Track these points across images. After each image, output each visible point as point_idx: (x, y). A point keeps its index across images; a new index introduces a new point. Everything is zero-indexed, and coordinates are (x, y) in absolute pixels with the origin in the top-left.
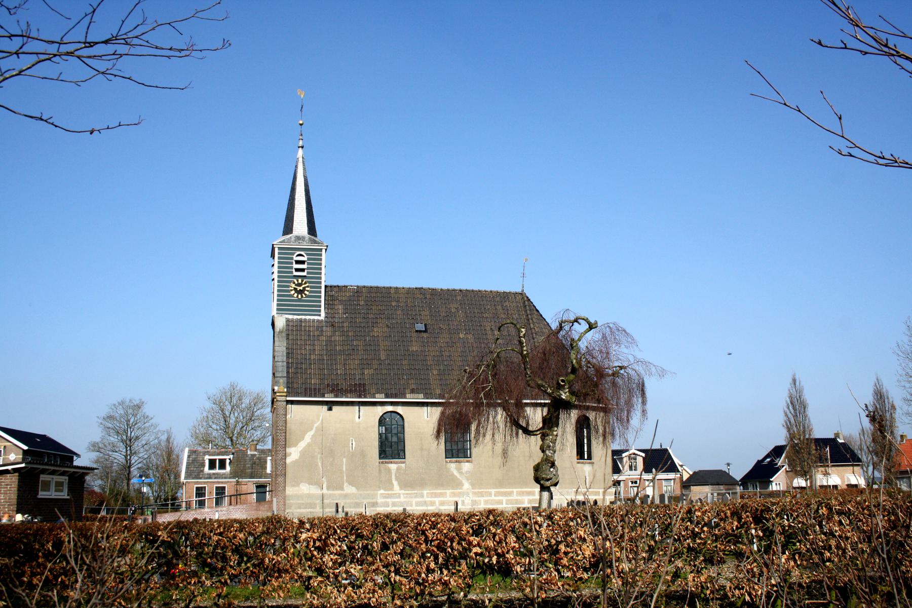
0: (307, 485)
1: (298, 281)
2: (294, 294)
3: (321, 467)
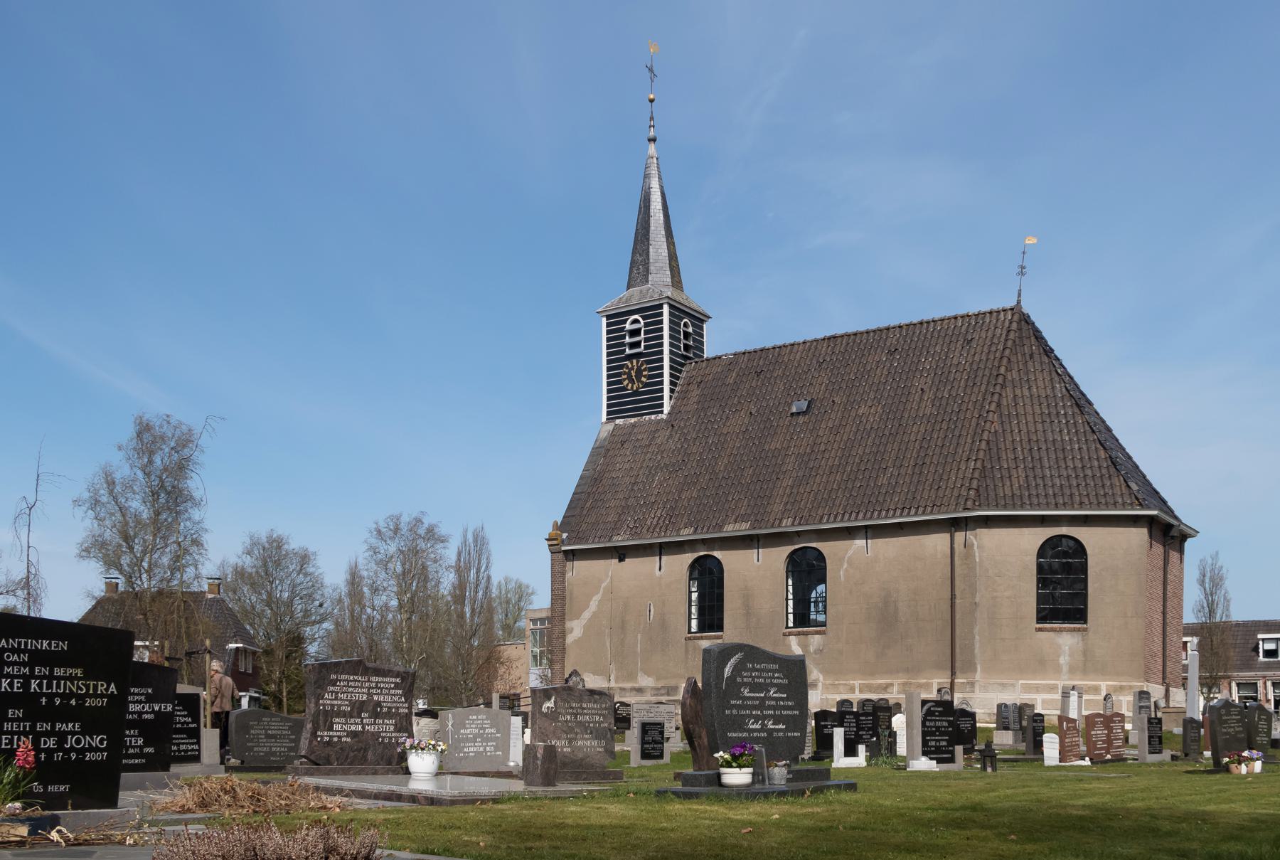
0: (592, 675)
2: (628, 385)
3: (609, 648)
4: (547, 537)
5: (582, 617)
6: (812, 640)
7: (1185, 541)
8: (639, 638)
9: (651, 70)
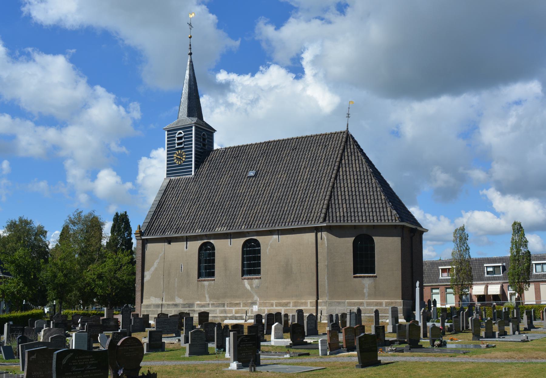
1: (178, 152)
2: (176, 162)
4: (135, 233)
5: (150, 270)
6: (254, 282)
7: (423, 234)
8: (176, 280)
9: (190, 25)
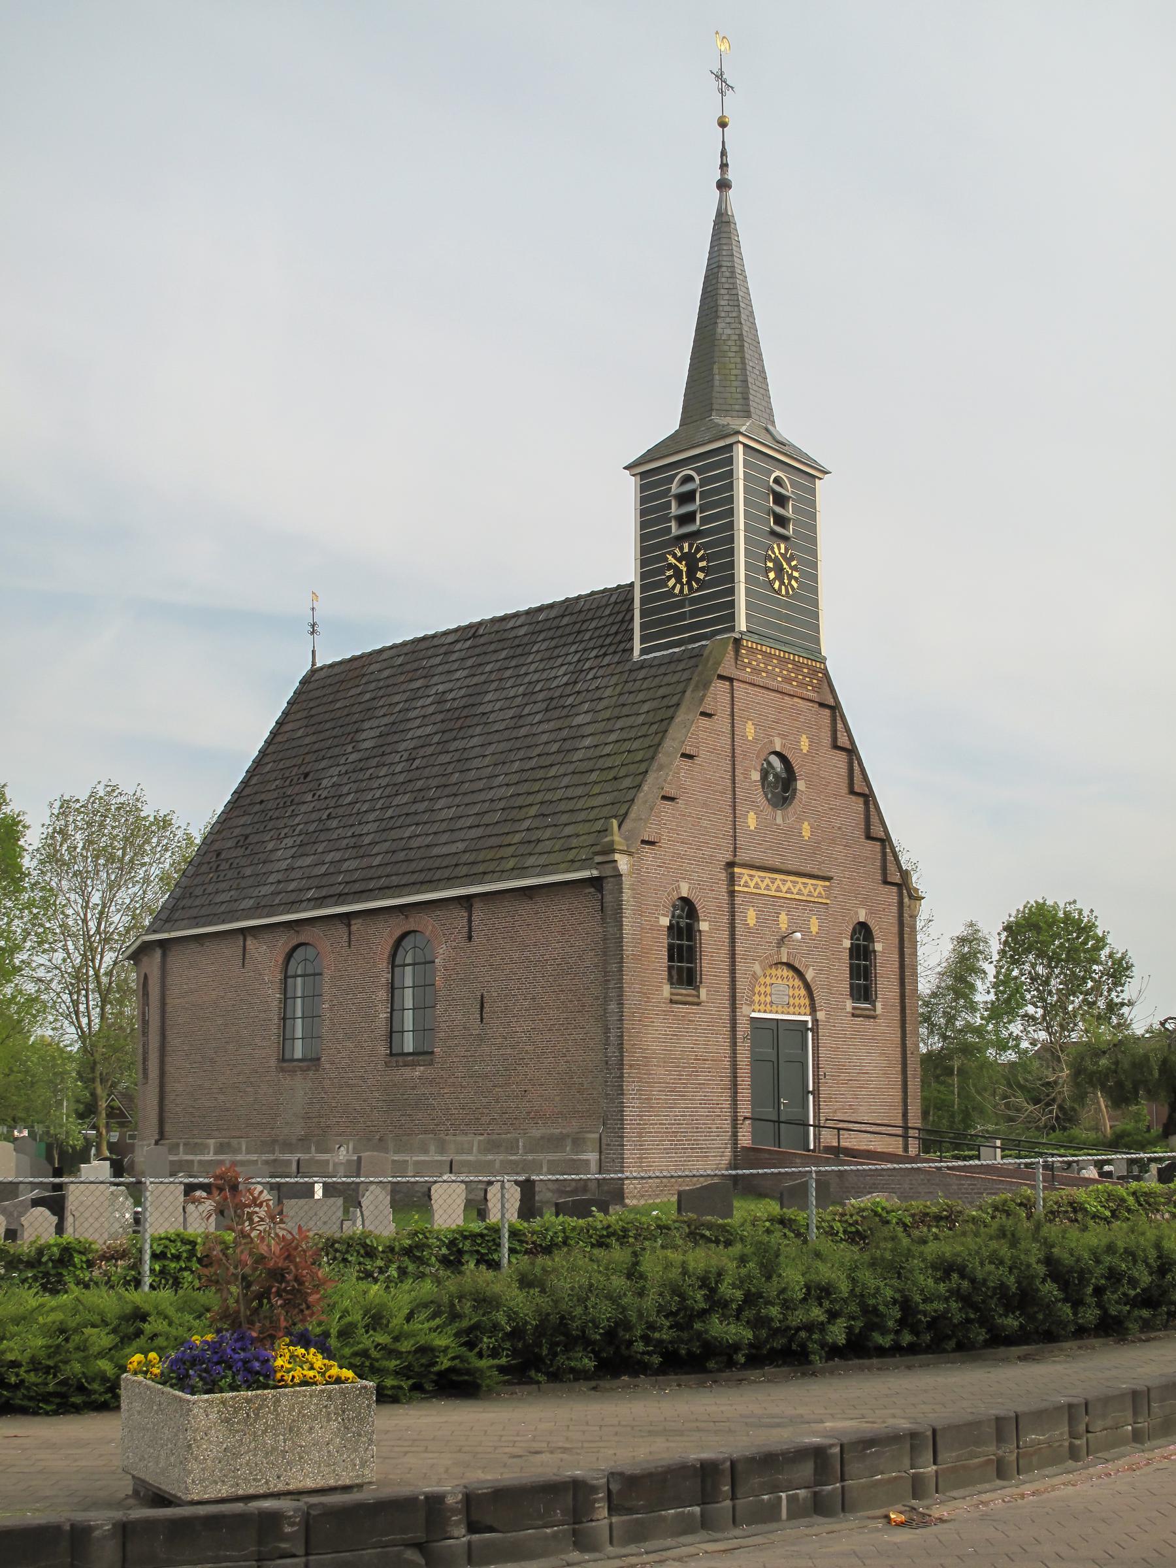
2: (674, 587)
9: (720, 76)
